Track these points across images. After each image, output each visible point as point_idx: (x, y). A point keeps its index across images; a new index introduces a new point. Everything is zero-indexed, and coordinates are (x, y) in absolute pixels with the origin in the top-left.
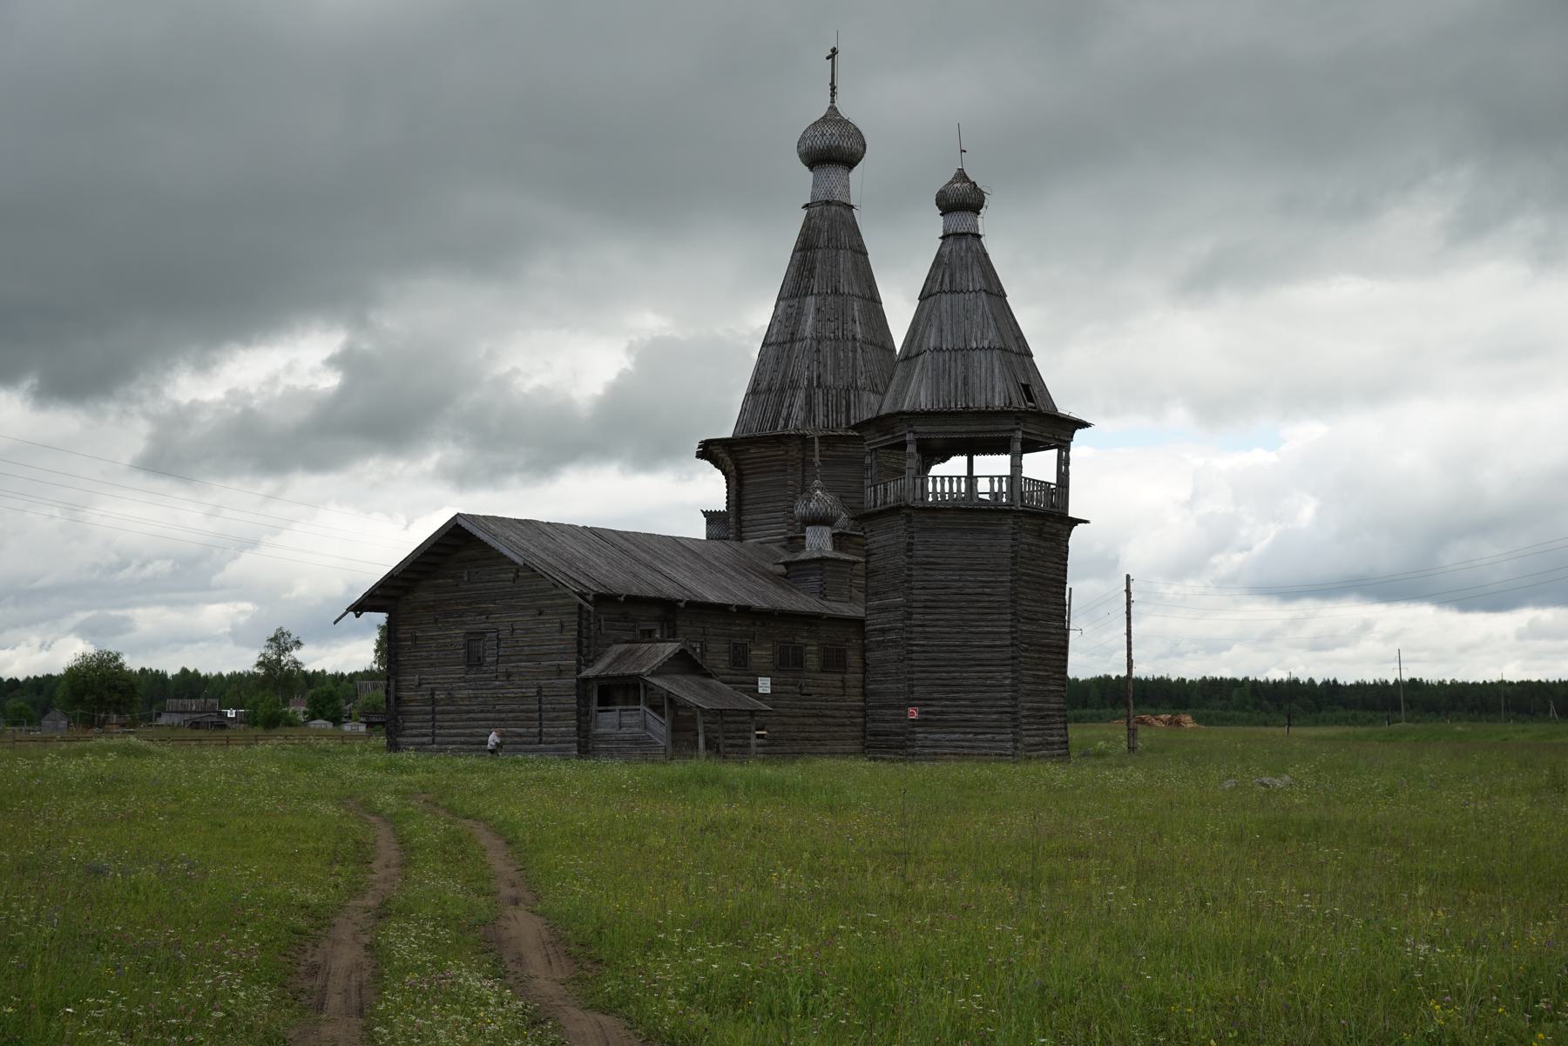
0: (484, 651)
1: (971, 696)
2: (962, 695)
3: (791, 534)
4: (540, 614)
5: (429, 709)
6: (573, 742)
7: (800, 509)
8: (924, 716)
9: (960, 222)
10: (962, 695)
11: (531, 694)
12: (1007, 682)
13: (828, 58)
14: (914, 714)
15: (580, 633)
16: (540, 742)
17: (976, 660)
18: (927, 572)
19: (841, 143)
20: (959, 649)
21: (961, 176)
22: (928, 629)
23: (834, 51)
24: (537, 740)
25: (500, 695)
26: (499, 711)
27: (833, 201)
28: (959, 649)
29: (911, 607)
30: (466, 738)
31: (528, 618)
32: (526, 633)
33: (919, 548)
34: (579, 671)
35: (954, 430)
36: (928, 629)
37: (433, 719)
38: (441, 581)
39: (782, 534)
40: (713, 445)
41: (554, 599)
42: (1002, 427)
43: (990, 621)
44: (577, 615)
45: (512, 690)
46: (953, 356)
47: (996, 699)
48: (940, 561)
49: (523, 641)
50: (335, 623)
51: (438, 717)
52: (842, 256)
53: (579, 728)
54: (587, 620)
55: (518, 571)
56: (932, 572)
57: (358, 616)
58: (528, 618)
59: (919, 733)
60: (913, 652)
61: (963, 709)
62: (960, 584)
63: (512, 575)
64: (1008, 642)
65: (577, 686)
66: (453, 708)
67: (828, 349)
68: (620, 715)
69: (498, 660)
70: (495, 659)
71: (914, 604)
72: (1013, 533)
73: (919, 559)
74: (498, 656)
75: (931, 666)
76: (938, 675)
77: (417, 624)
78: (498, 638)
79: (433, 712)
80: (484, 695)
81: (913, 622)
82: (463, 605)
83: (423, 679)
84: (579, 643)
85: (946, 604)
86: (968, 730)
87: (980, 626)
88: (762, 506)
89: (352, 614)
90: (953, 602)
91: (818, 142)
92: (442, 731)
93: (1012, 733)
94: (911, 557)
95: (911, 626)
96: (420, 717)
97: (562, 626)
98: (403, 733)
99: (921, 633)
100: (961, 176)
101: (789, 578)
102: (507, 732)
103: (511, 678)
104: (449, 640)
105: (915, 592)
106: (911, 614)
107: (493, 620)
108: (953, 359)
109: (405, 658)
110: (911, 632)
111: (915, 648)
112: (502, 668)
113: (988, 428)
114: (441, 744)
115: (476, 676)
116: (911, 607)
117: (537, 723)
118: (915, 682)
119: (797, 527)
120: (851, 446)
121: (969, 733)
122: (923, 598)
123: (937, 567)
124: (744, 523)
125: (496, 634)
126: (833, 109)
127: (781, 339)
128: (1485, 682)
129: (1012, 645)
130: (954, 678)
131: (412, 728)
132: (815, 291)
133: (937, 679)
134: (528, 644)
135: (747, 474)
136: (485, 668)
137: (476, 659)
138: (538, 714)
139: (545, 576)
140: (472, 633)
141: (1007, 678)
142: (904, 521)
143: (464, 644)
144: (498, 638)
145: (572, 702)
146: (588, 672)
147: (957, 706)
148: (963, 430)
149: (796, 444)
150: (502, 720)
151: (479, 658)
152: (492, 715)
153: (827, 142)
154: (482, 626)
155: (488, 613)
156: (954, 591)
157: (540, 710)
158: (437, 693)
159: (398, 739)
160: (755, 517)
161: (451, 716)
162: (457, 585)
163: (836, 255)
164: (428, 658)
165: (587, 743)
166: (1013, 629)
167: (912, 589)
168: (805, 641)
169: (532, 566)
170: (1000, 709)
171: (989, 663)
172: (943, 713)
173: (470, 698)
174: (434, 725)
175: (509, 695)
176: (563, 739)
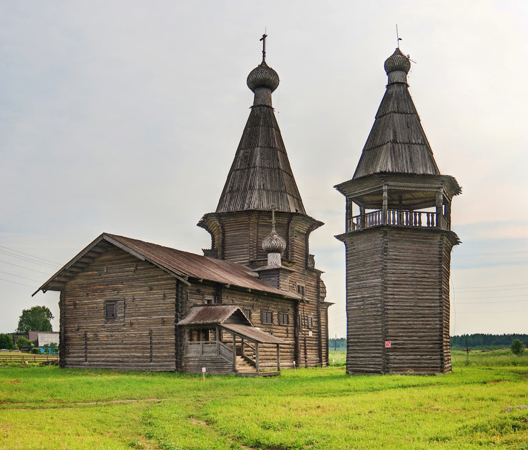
0: (116, 311)
1: (419, 334)
2: (414, 334)
3: (251, 260)
4: (150, 290)
5: (83, 342)
6: (172, 361)
7: (265, 244)
8: (394, 346)
9: (397, 76)
10: (414, 334)
11: (145, 335)
12: (438, 326)
13: (261, 40)
14: (388, 345)
15: (177, 300)
16: (151, 361)
17: (421, 314)
18: (396, 265)
19: (270, 77)
20: (412, 308)
21: (398, 51)
22: (396, 297)
23: (265, 36)
24: (149, 360)
25: (126, 335)
26: (125, 344)
27: (265, 105)
28: (412, 308)
29: (387, 284)
30: (105, 359)
31: (143, 292)
32: (142, 300)
33: (391, 250)
34: (177, 321)
35: (409, 185)
36: (396, 297)
37: (86, 348)
38: (90, 273)
39: (247, 260)
40: (211, 216)
41: (160, 281)
42: (434, 186)
43: (429, 293)
44: (175, 290)
45: (134, 332)
46: (403, 146)
47: (432, 336)
48: (402, 258)
49: (140, 305)
50: (33, 296)
51: (88, 347)
52: (270, 130)
53: (176, 354)
54: (181, 292)
55: (137, 266)
56: (398, 264)
57: (44, 292)
58: (143, 292)
59: (392, 355)
60: (388, 309)
61: (415, 342)
62: (413, 272)
63: (134, 268)
64: (438, 305)
65: (176, 330)
66: (98, 342)
67: (267, 172)
68: (203, 346)
69: (124, 316)
70: (123, 315)
71: (388, 282)
72: (440, 245)
73: (391, 257)
74: (125, 313)
75: (397, 318)
76: (401, 323)
77: (76, 297)
78: (125, 304)
79: (86, 344)
80: (117, 335)
81: (387, 292)
82: (104, 286)
83: (80, 326)
84: (177, 306)
85: (404, 283)
86: (417, 354)
87: (423, 295)
88: (235, 246)
89: (41, 291)
90: (409, 281)
91: (259, 76)
92: (91, 355)
93: (440, 355)
94: (386, 255)
95: (387, 294)
96: (79, 347)
97: (165, 296)
98: (68, 355)
99: (392, 299)
100: (398, 51)
101: (260, 279)
102: (131, 355)
103: (133, 326)
104: (95, 305)
105: (389, 275)
106: (386, 288)
107: (122, 294)
108: (403, 148)
109: (70, 315)
110: (387, 298)
111: (389, 307)
112: (128, 320)
113: (427, 185)
114: (90, 361)
115: (112, 324)
116: (387, 284)
117: (149, 350)
118: (389, 327)
119: (254, 256)
120: (281, 218)
121: (418, 355)
122: (393, 279)
123: (400, 261)
124: (226, 255)
125: (124, 301)
126: (264, 62)
127: (242, 167)
128: (505, 334)
129: (440, 306)
130: (410, 324)
131: (73, 353)
132: (260, 145)
133: (401, 325)
134: (143, 306)
135: (228, 231)
136: (116, 320)
137: (111, 315)
138: (150, 345)
139: (160, 267)
140: (108, 301)
141: (436, 324)
142: (382, 235)
143: (104, 307)
144: (125, 304)
145: (173, 339)
146: (181, 322)
147: (411, 340)
148: (414, 186)
149: (255, 216)
150: (128, 348)
151: (113, 315)
152: (121, 346)
153: (264, 76)
154: (115, 297)
155: (118, 290)
156: (409, 275)
157: (151, 343)
158: (88, 334)
159: (65, 359)
160: (231, 251)
161: (96, 347)
162: (100, 275)
163: (268, 129)
164: (82, 315)
165: (181, 362)
166: (441, 298)
167: (387, 273)
168: (273, 309)
169: (150, 261)
170: (434, 342)
171: (428, 316)
172: (404, 344)
173: (108, 336)
174: (86, 351)
175: (132, 335)
176: (165, 359)
